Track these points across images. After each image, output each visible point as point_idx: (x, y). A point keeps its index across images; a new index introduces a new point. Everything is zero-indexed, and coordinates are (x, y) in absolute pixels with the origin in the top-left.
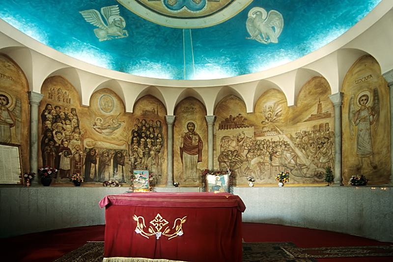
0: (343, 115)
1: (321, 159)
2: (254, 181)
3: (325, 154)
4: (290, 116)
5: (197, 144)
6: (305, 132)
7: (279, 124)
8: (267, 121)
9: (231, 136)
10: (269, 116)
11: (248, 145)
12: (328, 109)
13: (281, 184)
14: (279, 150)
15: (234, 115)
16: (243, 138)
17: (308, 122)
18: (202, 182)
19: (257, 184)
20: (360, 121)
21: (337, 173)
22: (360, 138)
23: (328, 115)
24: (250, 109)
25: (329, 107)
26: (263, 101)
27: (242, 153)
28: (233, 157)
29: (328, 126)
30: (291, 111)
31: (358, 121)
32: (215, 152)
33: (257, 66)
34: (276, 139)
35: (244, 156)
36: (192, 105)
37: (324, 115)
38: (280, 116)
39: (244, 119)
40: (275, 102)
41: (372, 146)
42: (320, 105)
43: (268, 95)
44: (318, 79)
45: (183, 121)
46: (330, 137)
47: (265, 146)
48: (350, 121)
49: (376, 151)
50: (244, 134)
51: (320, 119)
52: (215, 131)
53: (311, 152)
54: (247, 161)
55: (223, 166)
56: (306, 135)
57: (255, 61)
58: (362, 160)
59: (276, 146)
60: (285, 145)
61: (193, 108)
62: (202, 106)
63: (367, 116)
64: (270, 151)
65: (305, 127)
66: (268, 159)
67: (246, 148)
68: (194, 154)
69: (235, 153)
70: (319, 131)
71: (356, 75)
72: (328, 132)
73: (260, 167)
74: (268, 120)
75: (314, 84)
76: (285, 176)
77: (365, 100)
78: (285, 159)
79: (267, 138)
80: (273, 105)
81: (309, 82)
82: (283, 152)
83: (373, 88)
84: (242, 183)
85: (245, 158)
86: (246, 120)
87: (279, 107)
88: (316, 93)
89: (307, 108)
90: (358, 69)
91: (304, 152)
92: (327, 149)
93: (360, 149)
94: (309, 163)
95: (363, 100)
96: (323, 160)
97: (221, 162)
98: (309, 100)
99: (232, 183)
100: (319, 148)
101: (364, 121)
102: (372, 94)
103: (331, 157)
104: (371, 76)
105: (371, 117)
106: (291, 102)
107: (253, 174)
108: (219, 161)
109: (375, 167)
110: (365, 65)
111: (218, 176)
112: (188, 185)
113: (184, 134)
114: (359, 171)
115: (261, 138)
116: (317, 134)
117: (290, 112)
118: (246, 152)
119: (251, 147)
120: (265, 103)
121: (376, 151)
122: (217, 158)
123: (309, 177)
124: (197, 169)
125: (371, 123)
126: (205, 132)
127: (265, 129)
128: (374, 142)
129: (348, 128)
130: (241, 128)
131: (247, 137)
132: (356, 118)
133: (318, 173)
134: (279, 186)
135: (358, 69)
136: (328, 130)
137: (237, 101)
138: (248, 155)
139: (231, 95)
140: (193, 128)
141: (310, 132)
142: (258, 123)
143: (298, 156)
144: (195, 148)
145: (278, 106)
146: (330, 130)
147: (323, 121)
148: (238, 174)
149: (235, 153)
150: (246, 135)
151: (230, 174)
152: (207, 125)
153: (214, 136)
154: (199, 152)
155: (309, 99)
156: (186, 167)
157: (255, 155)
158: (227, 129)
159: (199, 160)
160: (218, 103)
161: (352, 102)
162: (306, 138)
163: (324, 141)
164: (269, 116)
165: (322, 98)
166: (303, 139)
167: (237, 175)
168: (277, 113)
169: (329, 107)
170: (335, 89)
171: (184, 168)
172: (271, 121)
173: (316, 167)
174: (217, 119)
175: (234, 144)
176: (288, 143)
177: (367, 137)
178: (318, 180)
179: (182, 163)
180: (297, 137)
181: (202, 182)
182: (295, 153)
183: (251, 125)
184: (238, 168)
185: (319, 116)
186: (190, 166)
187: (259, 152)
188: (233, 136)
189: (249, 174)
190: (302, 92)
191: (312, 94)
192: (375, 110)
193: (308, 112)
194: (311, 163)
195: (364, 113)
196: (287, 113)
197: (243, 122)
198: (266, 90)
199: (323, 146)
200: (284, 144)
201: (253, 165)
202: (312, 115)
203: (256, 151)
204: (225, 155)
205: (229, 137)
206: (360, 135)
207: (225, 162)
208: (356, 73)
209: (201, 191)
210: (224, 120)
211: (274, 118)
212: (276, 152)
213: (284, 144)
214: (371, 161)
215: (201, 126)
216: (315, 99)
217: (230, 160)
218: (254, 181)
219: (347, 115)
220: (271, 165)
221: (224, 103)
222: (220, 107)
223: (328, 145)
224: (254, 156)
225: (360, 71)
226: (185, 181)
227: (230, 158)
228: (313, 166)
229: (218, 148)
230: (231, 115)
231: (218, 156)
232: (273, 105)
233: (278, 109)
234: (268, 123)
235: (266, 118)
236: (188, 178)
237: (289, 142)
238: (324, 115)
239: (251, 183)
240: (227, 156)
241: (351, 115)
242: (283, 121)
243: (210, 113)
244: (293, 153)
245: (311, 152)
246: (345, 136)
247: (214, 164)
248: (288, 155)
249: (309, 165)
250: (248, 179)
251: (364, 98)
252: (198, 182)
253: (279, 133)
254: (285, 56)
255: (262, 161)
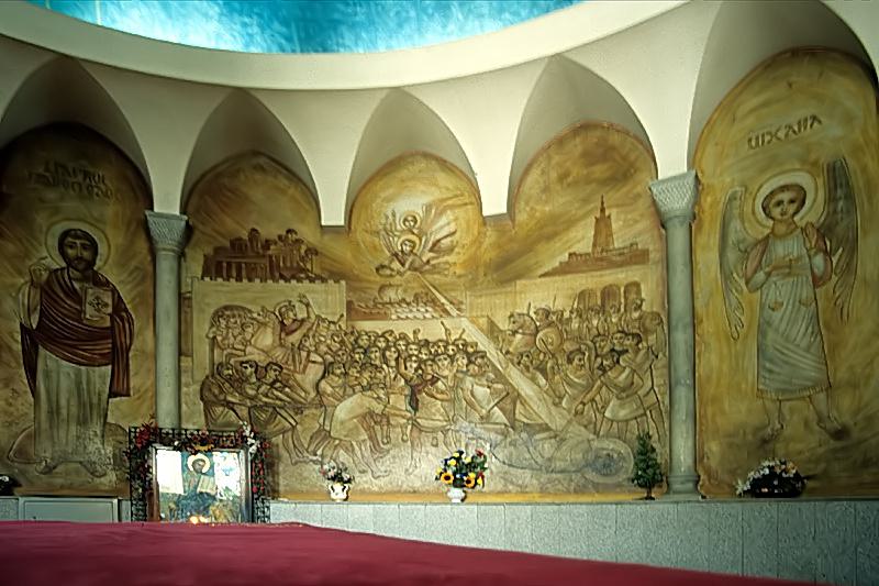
0: (699, 256)
1: (609, 409)
2: (349, 481)
3: (627, 391)
4: (488, 254)
5: (108, 324)
6: (547, 313)
7: (443, 279)
8: (396, 265)
9: (255, 308)
10: (407, 249)
11: (323, 348)
12: (640, 234)
13: (457, 493)
14: (446, 373)
15: (270, 231)
16: (303, 321)
17: (557, 278)
18: (132, 478)
19: (363, 492)
20: (768, 275)
21: (683, 453)
22: (771, 335)
23: (636, 257)
24: (333, 212)
25: (640, 226)
26: (383, 195)
27: (298, 377)
28: (264, 388)
29: (639, 292)
30: (491, 236)
31: (761, 276)
32: (186, 362)
33: (373, 43)
34: (434, 330)
35: (309, 387)
36: (84, 162)
37: (620, 254)
38: (451, 250)
39: (308, 250)
40: (426, 199)
41: (826, 358)
42: (603, 223)
43: (404, 173)
44: (598, 133)
45: (41, 219)
46: (646, 331)
47: (391, 355)
48: (726, 276)
49: (842, 374)
50: (308, 305)
51: (602, 269)
52: (187, 280)
53: (571, 384)
54: (321, 404)
55: (220, 420)
56: (549, 325)
57: (368, 15)
58: (780, 410)
59: (434, 358)
60: (469, 355)
61: (86, 174)
62: (130, 174)
63: (799, 258)
64: (410, 373)
65: (542, 295)
66: (400, 402)
67: (314, 357)
68: (91, 363)
69: (272, 375)
70: (602, 310)
71: (750, 121)
72: (636, 315)
73: (369, 429)
74: (403, 265)
75: (580, 149)
76: (471, 466)
77: (792, 201)
78: (469, 403)
79: (399, 327)
80: (420, 213)
81: (560, 142)
82: (462, 380)
83: (824, 160)
84: (304, 488)
85: (313, 394)
86: (317, 253)
87: (443, 220)
88: (588, 181)
89: (551, 229)
90: (755, 101)
91: (542, 381)
92: (634, 371)
93: (771, 371)
94: (564, 422)
95: (779, 203)
96: (616, 410)
97: (215, 404)
98: (560, 202)
99: (263, 481)
100: (602, 367)
101: (789, 274)
102: (820, 181)
103: (652, 399)
104: (814, 118)
105: (819, 260)
106: (495, 202)
107: (343, 456)
108: (202, 399)
109: (840, 434)
110: (790, 85)
111: (200, 456)
112: (62, 487)
113: (45, 275)
114: (769, 447)
115: (377, 326)
116: (595, 322)
117: (487, 242)
118: (314, 372)
119: (335, 354)
120: (389, 200)
121: (842, 374)
122: (197, 387)
123: (562, 472)
124: (105, 422)
125: (817, 282)
126: (143, 279)
127: (391, 295)
128: (834, 347)
129: (719, 299)
130: (294, 282)
131: (318, 317)
132: (751, 265)
133: (597, 457)
134: (449, 501)
135: (755, 101)
136: (640, 306)
137: (283, 182)
138: (323, 384)
139: (256, 153)
140: (86, 254)
141: (567, 315)
142: (365, 267)
143: (519, 395)
144: (96, 335)
145: (439, 214)
146: (644, 308)
147: (620, 277)
148: (285, 454)
149: (272, 375)
150: (315, 310)
151: (253, 449)
152: (153, 252)
153: (183, 300)
154: (118, 358)
155: (561, 200)
156: (54, 412)
157: (352, 387)
158: (239, 279)
159: (115, 389)
160: (203, 176)
161: (736, 212)
162: (548, 335)
163: (622, 344)
164: (407, 249)
165: (612, 197)
166: (540, 335)
167: (279, 457)
168: (439, 241)
169: (640, 226)
170: (671, 154)
171: (44, 416)
172: (413, 268)
173: (592, 436)
174: (197, 236)
175: (267, 339)
176: (481, 347)
177: (800, 331)
178: (601, 480)
179: (34, 392)
180: (515, 327)
181: (132, 478)
182: (506, 383)
183: (337, 276)
184: (284, 432)
185: (602, 258)
186: (74, 410)
187: (366, 375)
188: (263, 308)
189: (329, 453)
190: (535, 174)
191: (569, 185)
192: (835, 236)
193: (557, 244)
194: (569, 422)
195: (782, 250)
196: (477, 242)
197: (302, 259)
198: (394, 155)
199: (618, 362)
200: (466, 353)
201: (342, 423)
202: (570, 255)
203: (353, 372)
204: (229, 379)
205: (243, 309)
206: (769, 324)
207: (230, 405)
208: (752, 111)
209: (126, 519)
210: (228, 244)
211: (425, 259)
212: (434, 380)
213: (466, 353)
214: (819, 414)
215: (126, 255)
216: (586, 201)
217: (252, 398)
218: (349, 481)
219: (714, 256)
220: (415, 425)
221: (226, 181)
222: (204, 191)
223: (639, 359)
224: (347, 390)
225: (765, 104)
226: (49, 470)
227: (252, 392)
228: (578, 432)
229: (202, 350)
230: (254, 230)
231: (200, 376)
232: (420, 213)
233: (443, 227)
234: (399, 272)
235: (396, 255)
236: (66, 461)
237: (484, 344)
238: (620, 254)
239: (338, 487)
240: (238, 382)
241: (732, 256)
242: (459, 271)
243: (167, 199)
244: (500, 386)
245: (571, 384)
246: (707, 327)
247: (184, 407)
248: (482, 392)
249: (565, 429)
250: (325, 473)
251: (786, 196)
252: (111, 478)
253: (446, 311)
254: (491, 16)
255: (378, 408)
